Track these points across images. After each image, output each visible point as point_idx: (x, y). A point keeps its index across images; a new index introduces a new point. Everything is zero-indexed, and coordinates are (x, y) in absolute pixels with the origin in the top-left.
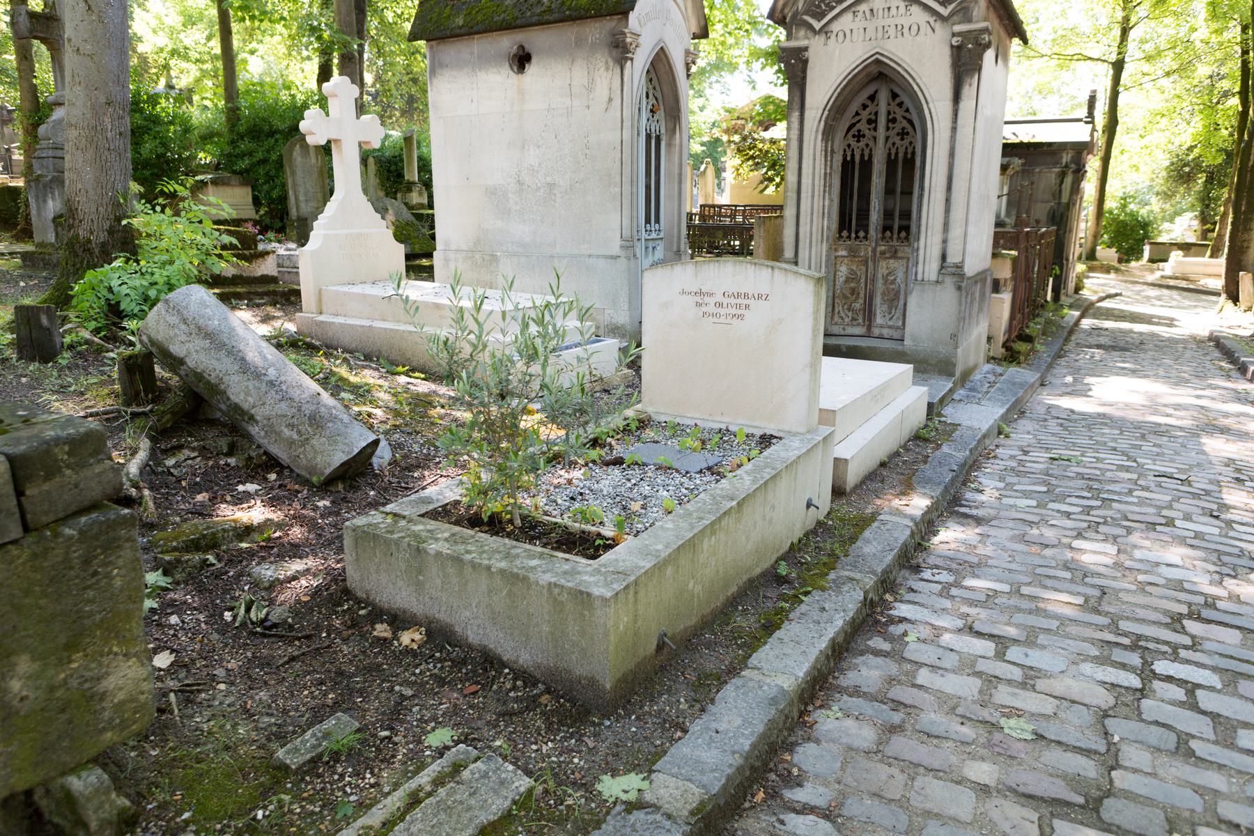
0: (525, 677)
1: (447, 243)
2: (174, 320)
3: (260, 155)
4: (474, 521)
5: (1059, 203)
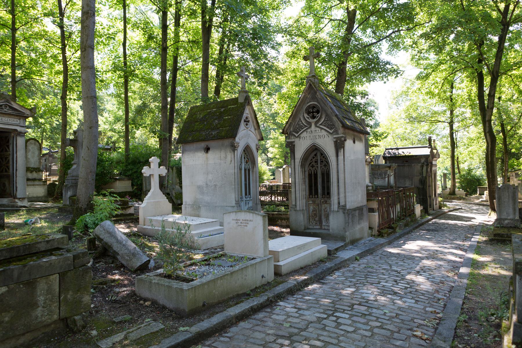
0: (171, 311)
1: (186, 202)
2: (101, 229)
3: (135, 170)
4: (165, 277)
5: (423, 177)
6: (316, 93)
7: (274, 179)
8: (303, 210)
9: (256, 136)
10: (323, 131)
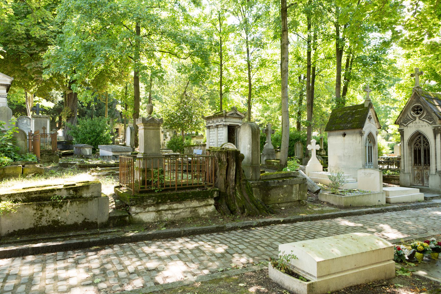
6: (420, 98)
7: (393, 153)
8: (409, 173)
9: (376, 126)
10: (424, 122)
